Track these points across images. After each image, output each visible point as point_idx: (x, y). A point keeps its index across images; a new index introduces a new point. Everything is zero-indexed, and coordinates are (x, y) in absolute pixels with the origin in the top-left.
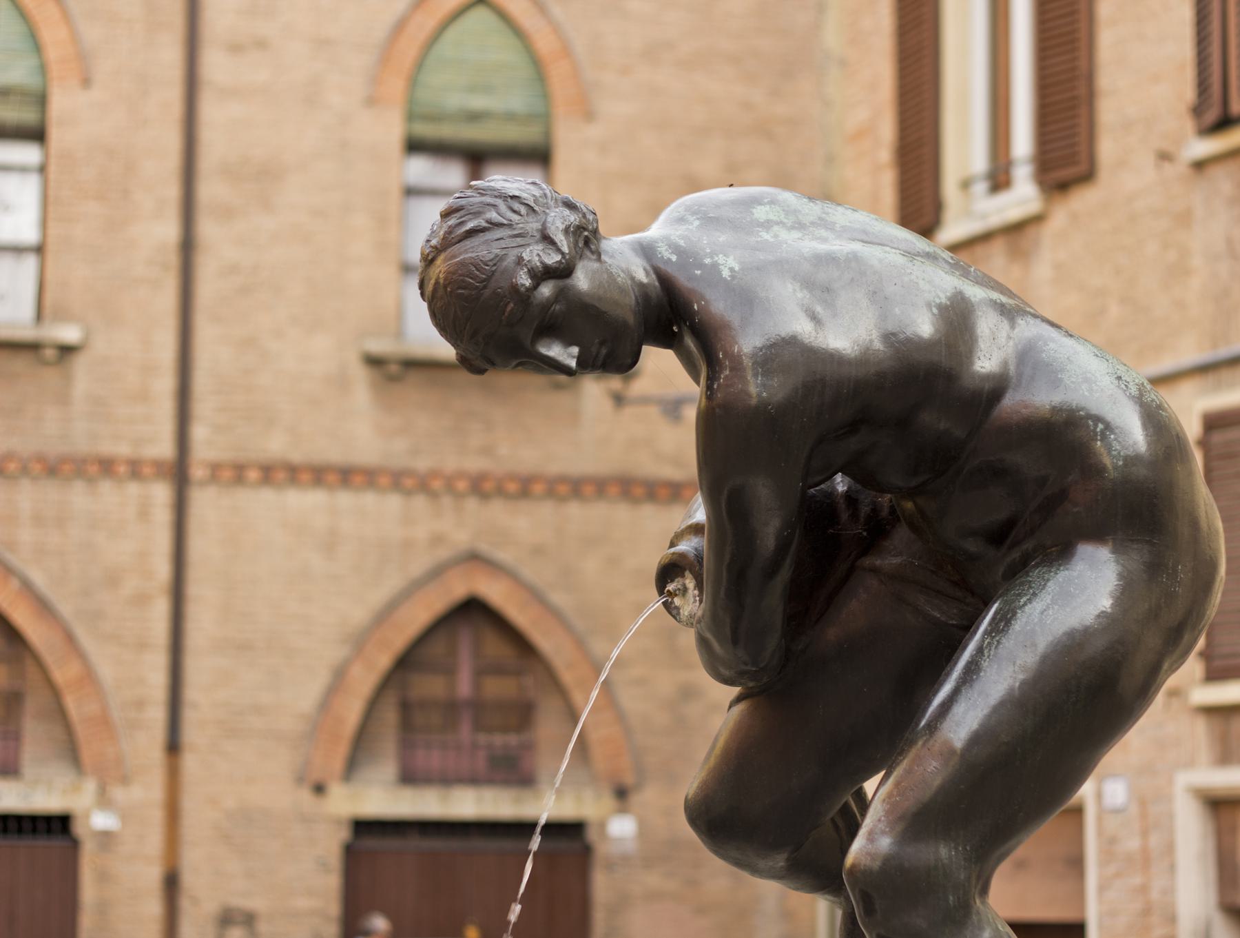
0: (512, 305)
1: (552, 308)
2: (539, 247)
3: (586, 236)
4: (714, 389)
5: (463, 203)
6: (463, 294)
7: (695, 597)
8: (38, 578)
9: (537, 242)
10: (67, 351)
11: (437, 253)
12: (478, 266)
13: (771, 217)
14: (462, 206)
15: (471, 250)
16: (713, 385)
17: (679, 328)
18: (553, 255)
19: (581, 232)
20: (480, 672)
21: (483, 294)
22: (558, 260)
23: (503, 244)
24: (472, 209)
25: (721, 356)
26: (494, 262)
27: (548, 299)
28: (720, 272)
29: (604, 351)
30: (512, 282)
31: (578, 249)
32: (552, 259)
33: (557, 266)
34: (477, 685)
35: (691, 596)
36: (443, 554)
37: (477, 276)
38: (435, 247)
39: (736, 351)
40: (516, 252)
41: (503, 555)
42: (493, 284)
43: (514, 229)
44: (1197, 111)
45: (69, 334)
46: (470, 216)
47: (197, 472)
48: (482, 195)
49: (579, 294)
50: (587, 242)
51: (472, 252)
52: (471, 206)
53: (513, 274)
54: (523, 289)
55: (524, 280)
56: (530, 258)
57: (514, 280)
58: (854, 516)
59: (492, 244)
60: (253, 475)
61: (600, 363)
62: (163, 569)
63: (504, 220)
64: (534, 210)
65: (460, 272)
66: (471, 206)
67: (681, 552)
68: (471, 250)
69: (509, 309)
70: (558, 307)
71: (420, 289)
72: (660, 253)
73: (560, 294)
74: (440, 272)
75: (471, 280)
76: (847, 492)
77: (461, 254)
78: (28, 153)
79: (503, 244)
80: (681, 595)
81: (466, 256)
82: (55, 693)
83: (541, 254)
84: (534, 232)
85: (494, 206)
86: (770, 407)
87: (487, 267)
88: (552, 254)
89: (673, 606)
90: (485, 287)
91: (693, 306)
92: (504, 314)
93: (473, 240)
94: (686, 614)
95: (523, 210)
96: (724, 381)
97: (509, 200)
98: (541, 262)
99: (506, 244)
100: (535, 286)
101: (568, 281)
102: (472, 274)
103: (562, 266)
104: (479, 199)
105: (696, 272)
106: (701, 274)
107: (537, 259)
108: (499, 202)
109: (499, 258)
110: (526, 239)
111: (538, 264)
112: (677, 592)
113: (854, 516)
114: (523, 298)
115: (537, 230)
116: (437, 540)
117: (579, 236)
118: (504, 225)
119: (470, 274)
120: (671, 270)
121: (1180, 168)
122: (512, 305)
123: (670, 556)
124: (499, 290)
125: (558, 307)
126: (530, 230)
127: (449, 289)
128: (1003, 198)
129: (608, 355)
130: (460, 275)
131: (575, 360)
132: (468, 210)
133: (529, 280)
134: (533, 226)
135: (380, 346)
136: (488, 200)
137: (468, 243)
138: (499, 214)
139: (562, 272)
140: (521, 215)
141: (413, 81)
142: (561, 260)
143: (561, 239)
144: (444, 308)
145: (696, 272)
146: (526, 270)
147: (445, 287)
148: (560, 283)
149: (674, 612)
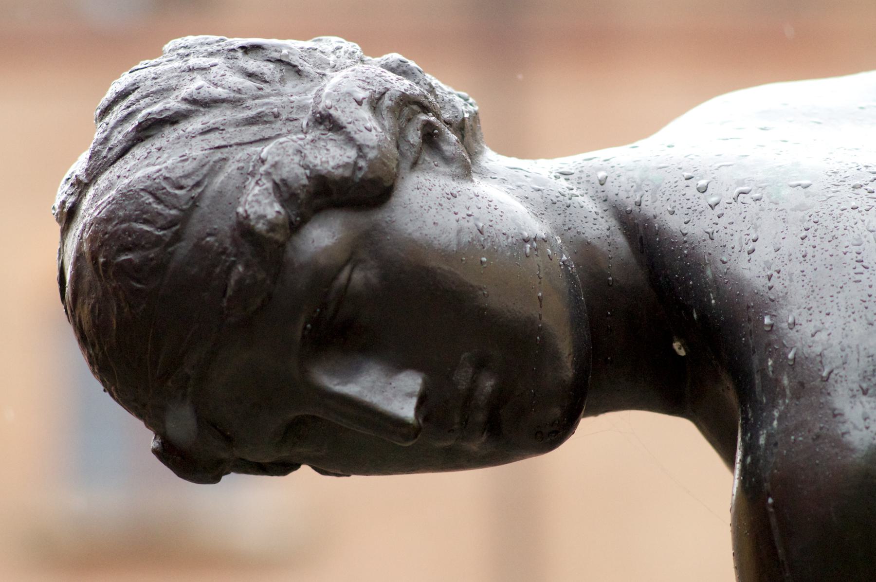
3: (428, 124)
4: (759, 447)
6: (130, 260)
11: (80, 193)
12: (159, 193)
16: (758, 438)
19: (415, 113)
21: (172, 254)
23: (215, 139)
26: (196, 179)
29: (488, 384)
37: (159, 214)
42: (195, 227)
54: (260, 226)
56: (277, 159)
65: (121, 213)
75: (146, 228)
87: (177, 192)
90: (177, 237)
95: (267, 69)
96: (779, 424)
101: (380, 216)
103: (360, 175)
122: (240, 268)
125: (358, 277)
127: (101, 260)
129: (499, 399)
131: (414, 401)
142: (356, 163)
146: (269, 185)
147: (94, 258)
148: (362, 220)
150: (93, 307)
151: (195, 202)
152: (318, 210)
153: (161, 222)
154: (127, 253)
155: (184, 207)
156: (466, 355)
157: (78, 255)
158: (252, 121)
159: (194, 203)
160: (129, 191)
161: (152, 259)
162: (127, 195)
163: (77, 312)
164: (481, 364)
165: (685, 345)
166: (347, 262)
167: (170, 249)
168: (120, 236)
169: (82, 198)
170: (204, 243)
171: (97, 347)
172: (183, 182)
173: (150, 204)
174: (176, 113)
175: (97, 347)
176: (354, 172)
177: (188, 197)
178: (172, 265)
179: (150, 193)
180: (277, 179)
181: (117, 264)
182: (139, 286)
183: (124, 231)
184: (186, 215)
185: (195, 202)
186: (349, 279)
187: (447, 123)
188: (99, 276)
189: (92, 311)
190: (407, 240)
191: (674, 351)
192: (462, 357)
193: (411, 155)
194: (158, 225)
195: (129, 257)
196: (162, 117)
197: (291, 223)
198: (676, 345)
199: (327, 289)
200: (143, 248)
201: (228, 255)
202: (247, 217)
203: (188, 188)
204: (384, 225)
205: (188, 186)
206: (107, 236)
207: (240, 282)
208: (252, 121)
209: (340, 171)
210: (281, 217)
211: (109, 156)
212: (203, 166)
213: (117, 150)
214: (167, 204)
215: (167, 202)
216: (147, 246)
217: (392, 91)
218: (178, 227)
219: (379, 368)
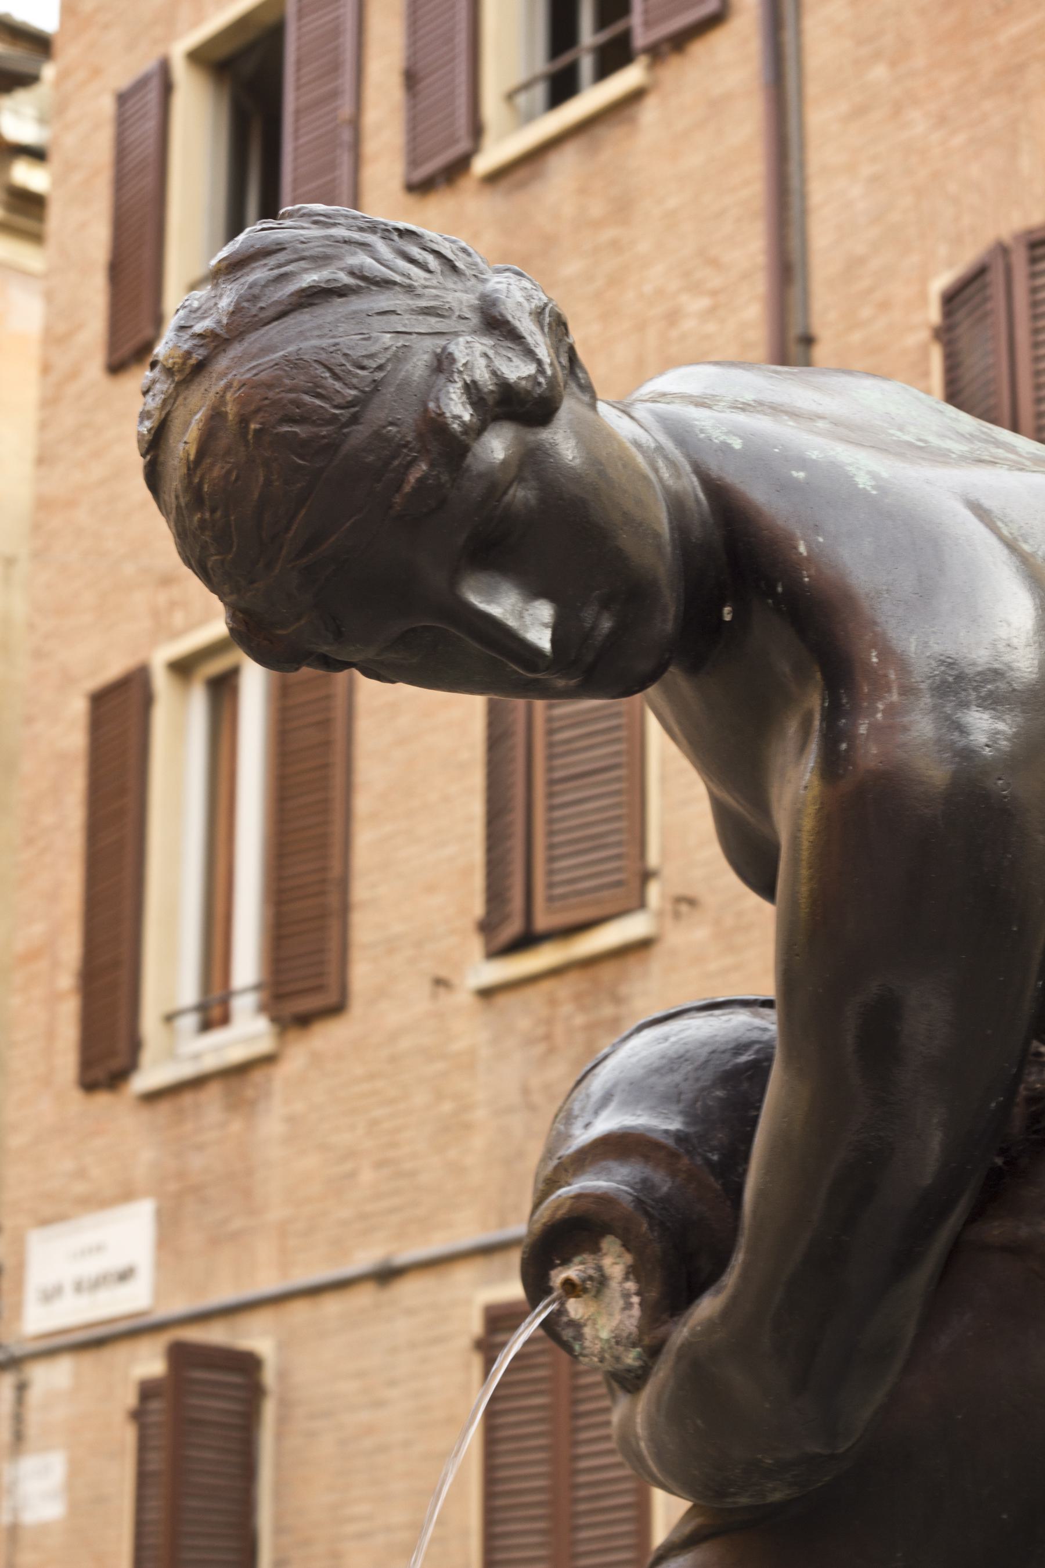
1: (511, 492)
2: (483, 344)
6: (295, 433)
7: (626, 1295)
11: (216, 347)
12: (337, 370)
15: (316, 333)
18: (517, 361)
21: (346, 435)
24: (303, 250)
25: (875, 660)
29: (606, 624)
30: (426, 410)
34: (630, 1358)
35: (617, 1295)
39: (913, 649)
42: (377, 414)
43: (419, 296)
44: (487, 927)
46: (303, 264)
51: (319, 337)
52: (303, 243)
53: (429, 391)
54: (456, 426)
56: (468, 358)
57: (432, 405)
59: (368, 320)
64: (454, 268)
66: (303, 243)
67: (599, 1192)
68: (316, 333)
69: (414, 476)
75: (318, 402)
77: (288, 342)
83: (491, 353)
84: (465, 309)
85: (364, 245)
87: (359, 372)
88: (514, 359)
89: (565, 1319)
90: (355, 419)
91: (796, 548)
92: (398, 488)
93: (318, 310)
94: (604, 1334)
95: (432, 262)
96: (884, 717)
97: (395, 236)
98: (494, 373)
99: (405, 326)
100: (478, 430)
101: (545, 435)
102: (322, 387)
103: (539, 391)
107: (482, 362)
110: (446, 321)
112: (589, 1284)
115: (471, 307)
118: (395, 283)
120: (732, 476)
121: (463, 996)
123: (569, 1203)
126: (455, 305)
127: (253, 426)
128: (217, 1037)
130: (291, 390)
132: (296, 251)
137: (304, 319)
140: (429, 271)
144: (233, 478)
146: (460, 384)
147: (243, 421)
150: (229, 472)
151: (377, 386)
152: (497, 418)
153: (339, 400)
154: (291, 425)
157: (213, 413)
158: (427, 311)
159: (376, 386)
160: (297, 359)
161: (324, 437)
164: (605, 605)
165: (734, 612)
167: (345, 430)
168: (285, 405)
169: (218, 353)
170: (384, 431)
171: (218, 514)
172: (366, 362)
173: (326, 378)
174: (345, 285)
177: (370, 379)
178: (345, 448)
180: (468, 379)
185: (377, 386)
190: (569, 466)
194: (335, 403)
196: (330, 287)
199: (497, 503)
200: (314, 423)
201: (411, 450)
202: (442, 414)
203: (372, 370)
205: (371, 368)
206: (266, 402)
207: (420, 480)
208: (427, 311)
212: (386, 349)
214: (347, 382)
215: (346, 380)
216: (319, 422)
218: (356, 409)
219: (516, 592)
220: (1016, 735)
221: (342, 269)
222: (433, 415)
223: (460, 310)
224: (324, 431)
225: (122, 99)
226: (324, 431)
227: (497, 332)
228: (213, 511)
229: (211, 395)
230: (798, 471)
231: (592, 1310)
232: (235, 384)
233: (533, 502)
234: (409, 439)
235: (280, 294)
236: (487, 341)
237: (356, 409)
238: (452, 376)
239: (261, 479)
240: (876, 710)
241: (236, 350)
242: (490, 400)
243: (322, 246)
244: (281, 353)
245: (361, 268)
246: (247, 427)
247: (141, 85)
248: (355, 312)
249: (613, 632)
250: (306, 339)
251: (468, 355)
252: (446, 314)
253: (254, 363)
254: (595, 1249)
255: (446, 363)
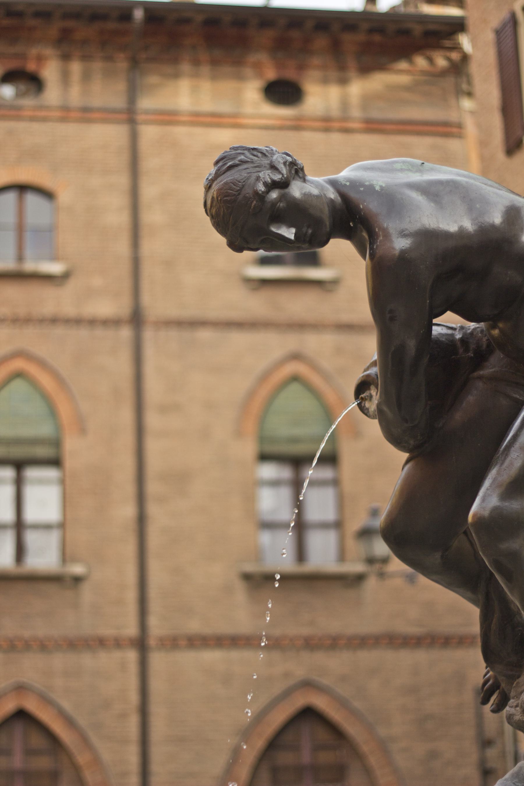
0: (255, 202)
3: (296, 169)
4: (374, 249)
5: (225, 154)
6: (227, 199)
8: (66, 705)
9: (268, 170)
10: (77, 580)
11: (212, 182)
13: (404, 167)
14: (225, 156)
16: (374, 246)
17: (354, 224)
18: (277, 175)
19: (293, 166)
20: (317, 748)
22: (280, 177)
23: (248, 171)
24: (230, 157)
26: (244, 180)
27: (275, 199)
28: (374, 188)
29: (310, 231)
30: (254, 189)
31: (291, 174)
32: (277, 177)
33: (280, 180)
36: (291, 682)
38: (212, 179)
39: (385, 226)
40: (256, 174)
41: (325, 681)
42: (244, 192)
43: (255, 164)
45: (78, 569)
46: (229, 160)
47: (152, 642)
48: (237, 150)
49: (294, 198)
50: (297, 172)
51: (231, 177)
52: (230, 155)
54: (260, 192)
55: (261, 188)
56: (264, 176)
57: (255, 188)
58: (467, 350)
60: (183, 643)
61: (308, 239)
62: (134, 697)
63: (248, 159)
65: (225, 188)
68: (230, 176)
70: (281, 205)
71: (204, 208)
72: (340, 182)
73: (282, 197)
74: (214, 191)
75: (231, 191)
76: (461, 338)
78: (51, 473)
79: (248, 171)
80: (369, 400)
81: (228, 179)
82: (76, 768)
84: (266, 165)
86: (406, 255)
87: (239, 183)
89: (365, 408)
90: (239, 194)
91: (360, 207)
92: (251, 207)
95: (259, 155)
97: (251, 150)
98: (270, 179)
99: (250, 171)
100: (268, 192)
101: (286, 190)
102: (232, 188)
103: (282, 181)
104: (234, 152)
105: (361, 189)
106: (363, 189)
107: (268, 177)
108: (246, 152)
109: (246, 178)
110: (261, 168)
111: (269, 180)
112: (367, 397)
113: (467, 350)
114: (261, 197)
115: (268, 164)
116: (287, 675)
117: (292, 168)
118: (249, 162)
119: (231, 188)
122: (255, 202)
124: (247, 195)
125: (281, 205)
127: (219, 199)
129: (312, 235)
130: (225, 190)
131: (294, 235)
133: (264, 187)
134: (265, 162)
135: (250, 568)
136: (239, 151)
138: (245, 157)
139: (284, 184)
141: (262, 419)
142: (281, 178)
143: (281, 167)
144: (217, 211)
145: (361, 189)
146: (262, 183)
147: (217, 198)
148: (282, 191)
149: (366, 411)
150: (216, 210)
151: (243, 186)
153: (235, 190)
155: (241, 187)
156: (306, 224)
158: (256, 167)
162: (226, 183)
163: (211, 211)
164: (309, 227)
166: (279, 201)
167: (237, 197)
170: (246, 196)
171: (216, 220)
172: (241, 181)
173: (232, 186)
175: (216, 220)
176: (281, 180)
179: (232, 183)
180: (264, 181)
181: (224, 200)
182: (229, 205)
183: (226, 192)
184: (240, 190)
185: (243, 186)
186: (279, 205)
187: (299, 168)
188: (218, 202)
189: (216, 211)
191: (350, 225)
192: (305, 225)
193: (293, 177)
195: (227, 198)
197: (267, 192)
198: (351, 224)
202: (257, 190)
204: (287, 193)
206: (221, 193)
207: (255, 205)
208: (256, 167)
209: (278, 180)
210: (265, 190)
211: (220, 174)
212: (245, 177)
213: (221, 173)
217: (288, 161)
218: (239, 192)
220: (411, 243)
221: (237, 160)
222: (255, 190)
223: (265, 165)
224: (233, 198)
225: (498, 33)
226: (233, 198)
227: (273, 169)
228: (215, 219)
229: (212, 193)
230: (361, 188)
231: (370, 404)
232: (215, 190)
233: (285, 206)
234: (251, 196)
235: (224, 169)
236: (269, 171)
237: (239, 192)
238: (260, 181)
239: (223, 211)
240: (377, 242)
241: (215, 183)
242: (269, 185)
243: (234, 155)
244: (224, 182)
245: (241, 159)
246: (218, 199)
247: (504, 26)
248: (239, 170)
249: (312, 233)
250: (228, 178)
251: (264, 175)
252: (261, 166)
253: (218, 185)
254: (369, 389)
255: (259, 178)
